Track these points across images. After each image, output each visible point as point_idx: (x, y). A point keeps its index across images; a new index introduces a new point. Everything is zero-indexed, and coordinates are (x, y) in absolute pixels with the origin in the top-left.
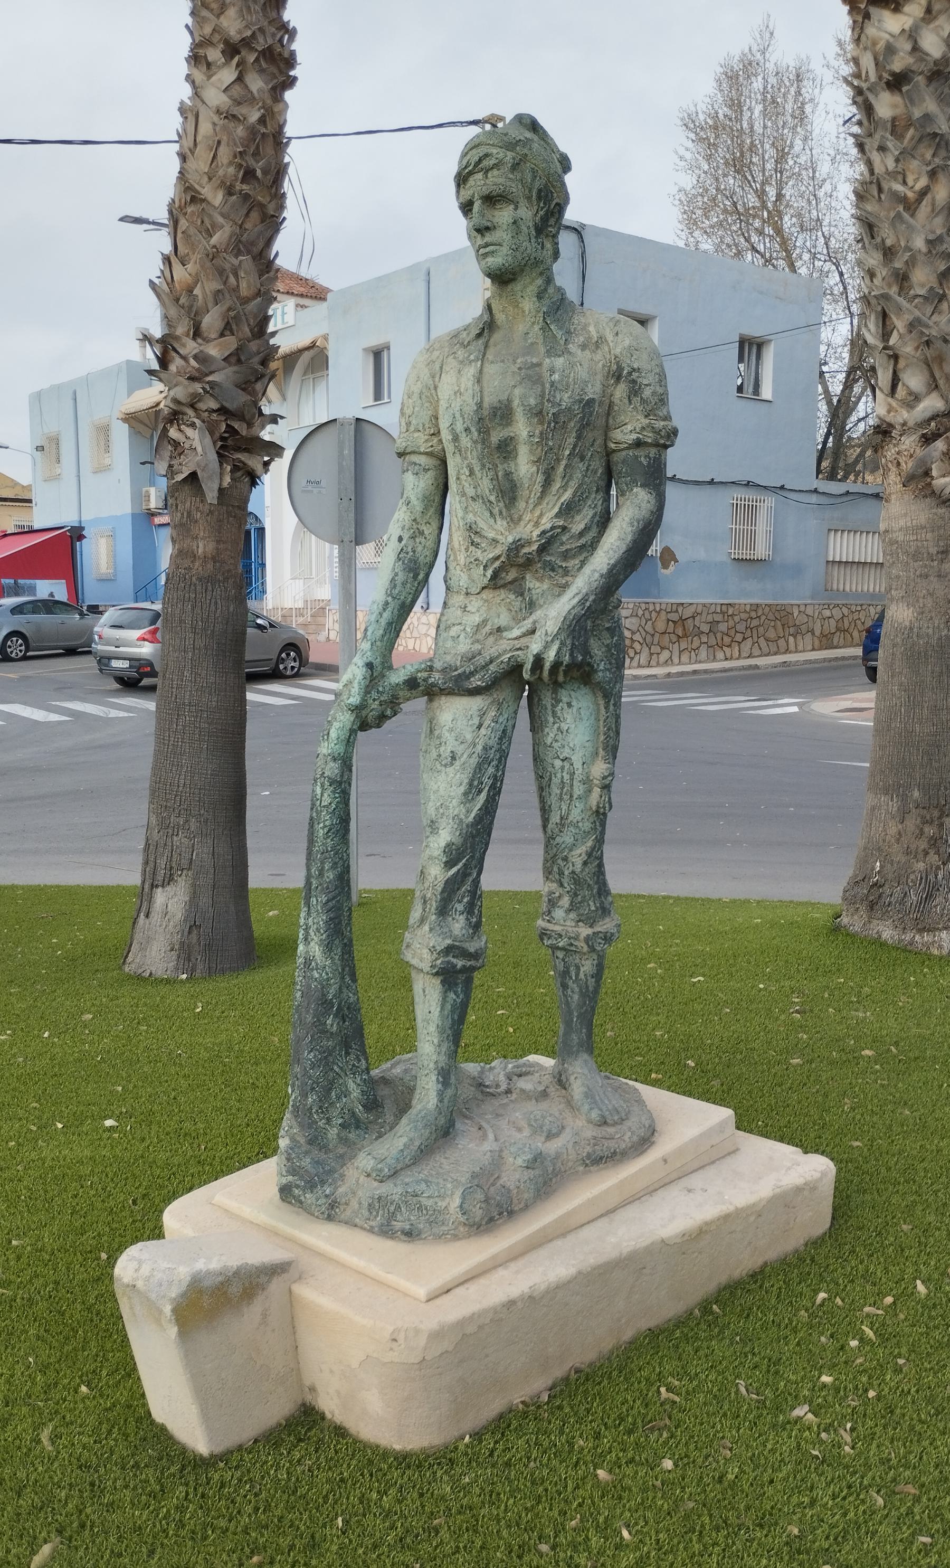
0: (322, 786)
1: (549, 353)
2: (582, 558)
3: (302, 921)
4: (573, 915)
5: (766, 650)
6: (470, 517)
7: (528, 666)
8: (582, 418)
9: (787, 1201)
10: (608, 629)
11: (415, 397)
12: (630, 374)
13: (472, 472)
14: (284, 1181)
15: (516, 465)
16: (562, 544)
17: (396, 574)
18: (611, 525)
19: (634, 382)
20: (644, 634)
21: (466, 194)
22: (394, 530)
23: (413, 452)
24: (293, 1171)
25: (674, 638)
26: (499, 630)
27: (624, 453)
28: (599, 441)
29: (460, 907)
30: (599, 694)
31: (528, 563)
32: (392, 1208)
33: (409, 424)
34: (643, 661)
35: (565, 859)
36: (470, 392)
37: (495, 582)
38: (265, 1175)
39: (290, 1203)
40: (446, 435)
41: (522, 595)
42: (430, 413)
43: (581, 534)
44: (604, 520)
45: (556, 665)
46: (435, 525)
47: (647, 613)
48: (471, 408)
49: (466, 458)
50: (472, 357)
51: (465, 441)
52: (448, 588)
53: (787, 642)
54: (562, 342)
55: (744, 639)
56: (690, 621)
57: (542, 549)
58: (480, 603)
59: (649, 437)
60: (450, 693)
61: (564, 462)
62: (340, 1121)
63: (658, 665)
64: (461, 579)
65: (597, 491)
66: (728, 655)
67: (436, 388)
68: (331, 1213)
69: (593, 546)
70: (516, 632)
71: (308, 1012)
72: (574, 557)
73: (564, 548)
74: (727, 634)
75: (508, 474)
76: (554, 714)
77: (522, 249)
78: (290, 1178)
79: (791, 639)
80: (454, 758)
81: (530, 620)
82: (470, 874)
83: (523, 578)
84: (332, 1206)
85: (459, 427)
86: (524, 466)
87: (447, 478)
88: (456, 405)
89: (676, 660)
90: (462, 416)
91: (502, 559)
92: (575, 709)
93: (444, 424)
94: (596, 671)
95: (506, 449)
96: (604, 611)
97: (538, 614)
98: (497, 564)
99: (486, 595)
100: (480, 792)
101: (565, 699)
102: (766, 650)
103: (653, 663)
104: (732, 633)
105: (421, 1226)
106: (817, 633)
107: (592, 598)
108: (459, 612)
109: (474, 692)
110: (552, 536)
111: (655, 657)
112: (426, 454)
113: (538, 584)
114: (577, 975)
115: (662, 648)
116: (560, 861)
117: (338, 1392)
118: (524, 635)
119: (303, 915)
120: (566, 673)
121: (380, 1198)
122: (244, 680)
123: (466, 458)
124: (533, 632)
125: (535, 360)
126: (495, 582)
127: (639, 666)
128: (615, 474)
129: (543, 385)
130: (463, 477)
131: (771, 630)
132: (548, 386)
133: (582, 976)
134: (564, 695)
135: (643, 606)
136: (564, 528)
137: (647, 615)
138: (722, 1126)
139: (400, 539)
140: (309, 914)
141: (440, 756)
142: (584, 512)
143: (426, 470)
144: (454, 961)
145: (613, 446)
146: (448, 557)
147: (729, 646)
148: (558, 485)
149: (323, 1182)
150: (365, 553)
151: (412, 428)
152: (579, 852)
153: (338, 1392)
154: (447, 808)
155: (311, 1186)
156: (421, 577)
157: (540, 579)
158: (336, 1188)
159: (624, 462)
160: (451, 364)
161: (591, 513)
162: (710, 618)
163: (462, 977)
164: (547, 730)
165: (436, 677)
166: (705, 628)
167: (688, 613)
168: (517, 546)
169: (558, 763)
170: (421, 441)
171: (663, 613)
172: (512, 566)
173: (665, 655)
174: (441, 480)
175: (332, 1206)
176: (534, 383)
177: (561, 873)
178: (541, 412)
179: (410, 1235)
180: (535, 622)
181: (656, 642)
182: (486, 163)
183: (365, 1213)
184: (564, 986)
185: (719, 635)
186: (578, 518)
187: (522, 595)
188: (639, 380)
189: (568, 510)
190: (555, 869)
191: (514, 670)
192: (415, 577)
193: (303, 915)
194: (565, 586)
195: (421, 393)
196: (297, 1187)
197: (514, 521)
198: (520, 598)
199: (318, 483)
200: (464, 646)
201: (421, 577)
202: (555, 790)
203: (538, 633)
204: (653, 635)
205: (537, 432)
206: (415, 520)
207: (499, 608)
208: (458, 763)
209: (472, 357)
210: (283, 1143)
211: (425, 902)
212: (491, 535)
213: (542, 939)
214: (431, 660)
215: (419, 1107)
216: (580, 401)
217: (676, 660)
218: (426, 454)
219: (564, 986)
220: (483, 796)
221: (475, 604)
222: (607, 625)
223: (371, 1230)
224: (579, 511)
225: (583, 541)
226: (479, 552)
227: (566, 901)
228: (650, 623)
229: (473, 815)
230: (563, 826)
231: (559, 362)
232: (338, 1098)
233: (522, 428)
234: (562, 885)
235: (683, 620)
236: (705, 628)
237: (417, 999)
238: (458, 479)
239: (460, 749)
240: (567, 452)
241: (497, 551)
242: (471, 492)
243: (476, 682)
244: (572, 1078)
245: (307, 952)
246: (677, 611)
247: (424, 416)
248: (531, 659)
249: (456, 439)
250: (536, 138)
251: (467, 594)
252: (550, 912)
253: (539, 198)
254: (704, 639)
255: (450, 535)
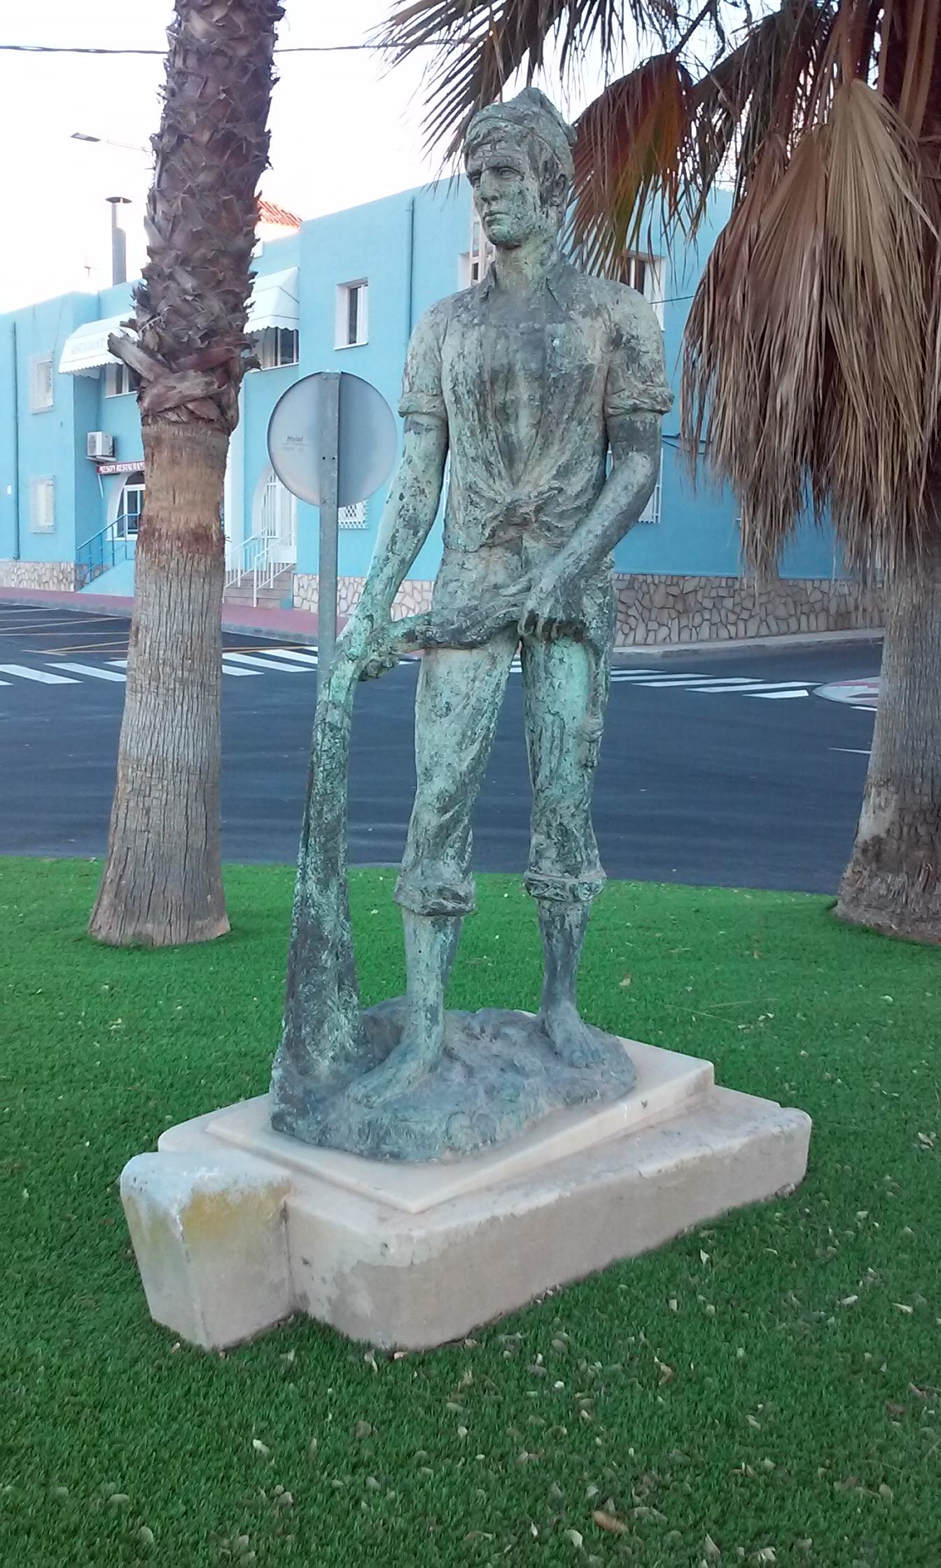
0: (323, 731)
1: (552, 320)
2: (577, 519)
3: (300, 861)
4: (558, 866)
5: (774, 628)
6: (470, 477)
7: (523, 622)
8: (582, 383)
9: (763, 1148)
10: (600, 588)
11: (419, 358)
12: (629, 341)
13: (473, 433)
14: (276, 1109)
15: (517, 427)
16: (559, 505)
17: (397, 531)
18: (607, 487)
19: (633, 349)
20: (640, 608)
21: (475, 164)
22: (392, 486)
23: (416, 412)
24: (284, 1099)
25: (674, 614)
26: (496, 587)
27: (621, 418)
28: (597, 407)
29: (451, 852)
30: (591, 652)
31: (524, 523)
32: (382, 1133)
33: (412, 384)
34: (639, 638)
35: (554, 811)
36: (473, 355)
37: (490, 544)
38: (261, 1107)
39: (282, 1131)
40: (448, 396)
41: (519, 554)
42: (433, 374)
43: (577, 496)
44: (601, 483)
45: (550, 622)
46: (435, 484)
47: (644, 586)
48: (471, 373)
49: (467, 420)
50: (476, 321)
51: (469, 403)
52: (446, 546)
53: (799, 621)
54: (564, 308)
55: (751, 616)
56: (691, 595)
57: (539, 510)
58: (478, 560)
59: (646, 402)
60: (447, 646)
61: (562, 427)
62: (331, 1054)
63: (655, 643)
64: (461, 538)
65: (593, 455)
66: (733, 634)
67: (440, 350)
68: (322, 1142)
69: (588, 508)
70: (513, 590)
71: (303, 947)
72: (570, 517)
73: (559, 510)
74: (733, 612)
75: (507, 438)
76: (547, 670)
77: (526, 218)
78: (283, 1106)
79: (804, 618)
80: (448, 709)
81: (526, 578)
82: (461, 821)
83: (521, 538)
84: (323, 1133)
85: (461, 389)
86: (523, 428)
87: (448, 438)
88: (459, 367)
89: (675, 637)
90: (465, 377)
91: (500, 518)
92: (566, 666)
93: (447, 386)
94: (588, 629)
95: (505, 413)
96: (597, 571)
97: (534, 572)
98: (495, 523)
99: (484, 553)
100: (473, 742)
101: (557, 655)
102: (774, 628)
103: (650, 641)
104: (738, 609)
105: (409, 1149)
106: (833, 610)
107: (586, 557)
108: (457, 569)
109: (471, 646)
110: (549, 498)
111: (652, 634)
112: (428, 414)
113: (534, 544)
114: (562, 925)
115: (660, 625)
116: (548, 813)
117: (329, 1300)
118: (520, 592)
119: (300, 855)
120: (558, 629)
121: (369, 1123)
122: (219, 644)
123: (467, 420)
124: (529, 589)
125: (537, 326)
126: (490, 544)
127: (635, 644)
128: (612, 439)
129: (544, 349)
130: (464, 438)
131: (782, 607)
132: (549, 351)
133: (566, 926)
134: (557, 651)
135: (641, 578)
136: (561, 490)
137: (644, 588)
138: (699, 1087)
139: (401, 497)
140: (306, 854)
141: (435, 706)
142: (581, 474)
143: (428, 430)
144: (445, 902)
145: (610, 411)
146: (447, 515)
147: (735, 624)
148: (556, 447)
149: (315, 1110)
150: (352, 517)
151: (415, 389)
152: (566, 804)
153: (329, 1300)
154: (441, 756)
155: (303, 1113)
156: (421, 534)
157: (537, 539)
158: (327, 1114)
159: (621, 426)
160: (456, 326)
161: (588, 475)
162: (714, 594)
163: (452, 919)
164: (538, 685)
165: (434, 631)
166: (708, 603)
167: (689, 586)
168: (511, 508)
169: (549, 718)
170: (425, 402)
171: (662, 586)
172: (509, 525)
173: (664, 632)
174: (443, 441)
175: (323, 1133)
176: (536, 348)
177: (549, 825)
178: (541, 377)
179: (397, 1157)
180: (530, 580)
181: (653, 617)
182: (495, 136)
183: (355, 1137)
184: (549, 936)
185: (723, 612)
186: (573, 480)
187: (519, 554)
188: (638, 348)
189: (564, 472)
190: (544, 821)
191: (510, 625)
192: (415, 534)
193: (300, 855)
194: (561, 546)
195: (425, 353)
196: (290, 1114)
197: (515, 482)
198: (516, 557)
199: (300, 439)
200: (462, 601)
201: (421, 534)
202: (546, 745)
203: (533, 590)
204: (650, 611)
205: (538, 396)
206: (416, 479)
207: (497, 567)
208: (452, 714)
209: (476, 321)
210: (276, 1074)
211: (418, 846)
212: (491, 494)
213: (528, 890)
214: (428, 614)
215: (408, 1041)
216: (580, 367)
217: (675, 637)
218: (428, 414)
219: (549, 936)
220: (476, 746)
221: (471, 562)
222: (600, 585)
223: (361, 1155)
224: (575, 474)
225: (578, 503)
226: (478, 511)
227: (553, 853)
228: (647, 597)
229: (466, 764)
230: (552, 778)
231: (561, 328)
232: (331, 1031)
233: (523, 391)
234: (549, 837)
235: (683, 596)
236: (708, 603)
237: (407, 940)
238: (459, 439)
239: (454, 701)
240: (566, 416)
241: (496, 512)
242: (471, 452)
243: (471, 636)
244: (555, 1025)
245: (304, 890)
246: (677, 584)
247: (426, 378)
248: (526, 615)
249: (458, 400)
250: (543, 112)
251: (465, 551)
252: (537, 863)
253: (546, 169)
254: (707, 616)
255: (450, 494)
